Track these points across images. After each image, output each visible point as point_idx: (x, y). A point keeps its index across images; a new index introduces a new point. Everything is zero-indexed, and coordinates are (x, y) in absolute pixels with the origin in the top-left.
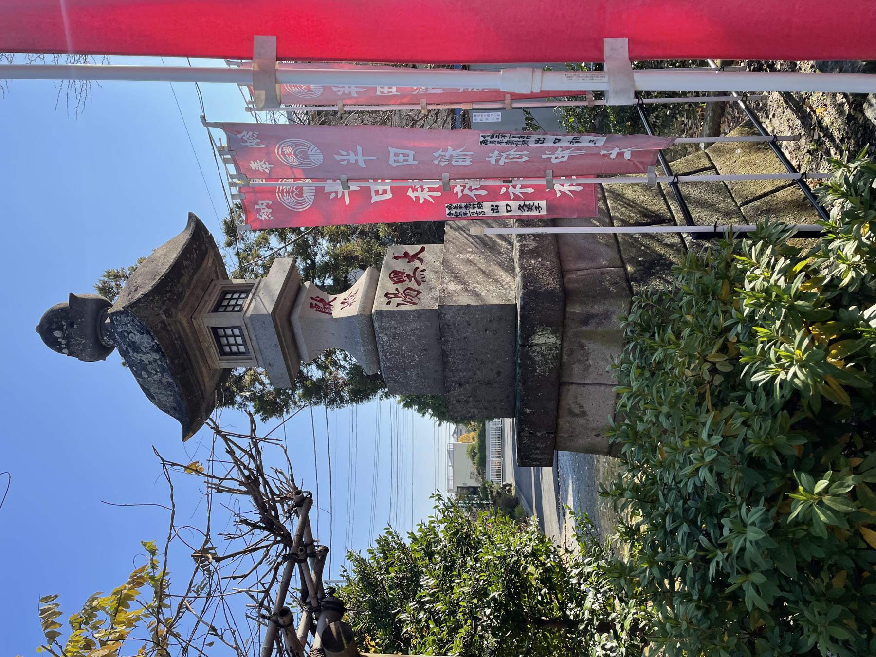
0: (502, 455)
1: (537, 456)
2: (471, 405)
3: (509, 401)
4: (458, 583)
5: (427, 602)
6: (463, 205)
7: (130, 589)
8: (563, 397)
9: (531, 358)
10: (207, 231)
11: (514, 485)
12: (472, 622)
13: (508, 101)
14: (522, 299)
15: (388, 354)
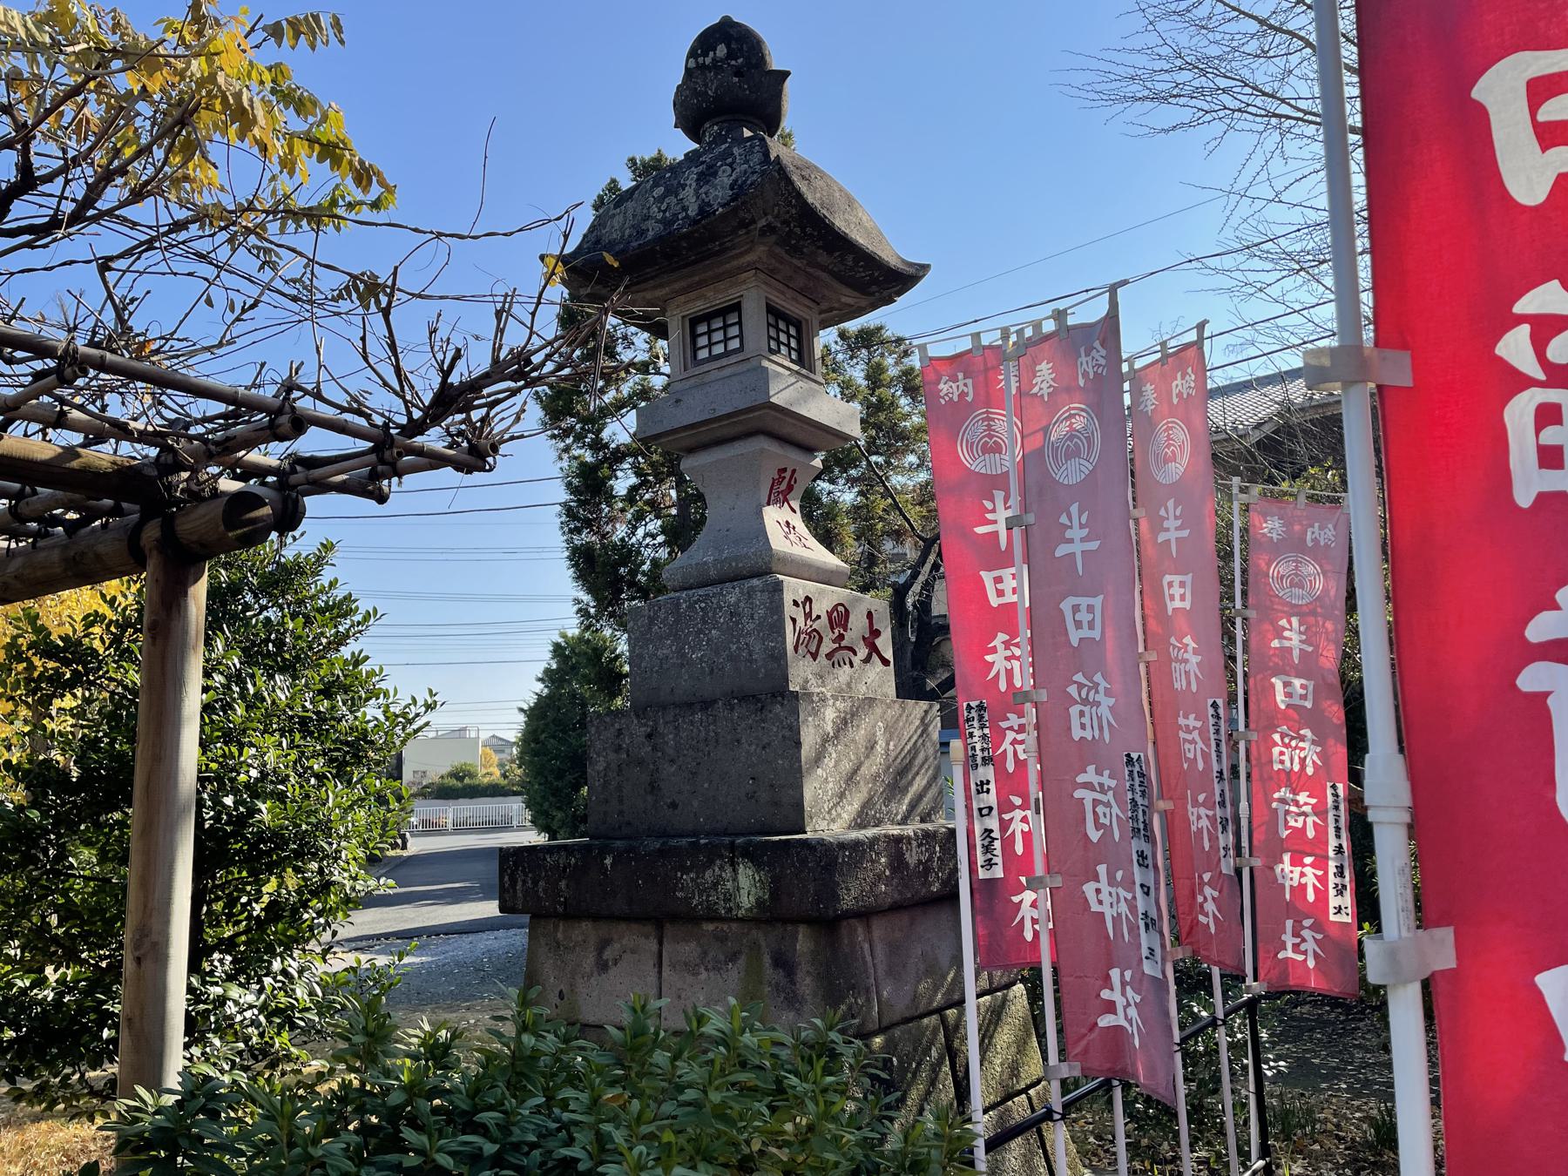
0: (460, 828)
1: (520, 883)
2: (612, 756)
3: (620, 827)
4: (280, 744)
5: (244, 689)
6: (987, 731)
7: (350, 163)
8: (634, 926)
9: (711, 863)
10: (900, 294)
11: (405, 854)
12: (212, 771)
13: (1162, 805)
14: (821, 842)
15: (703, 605)
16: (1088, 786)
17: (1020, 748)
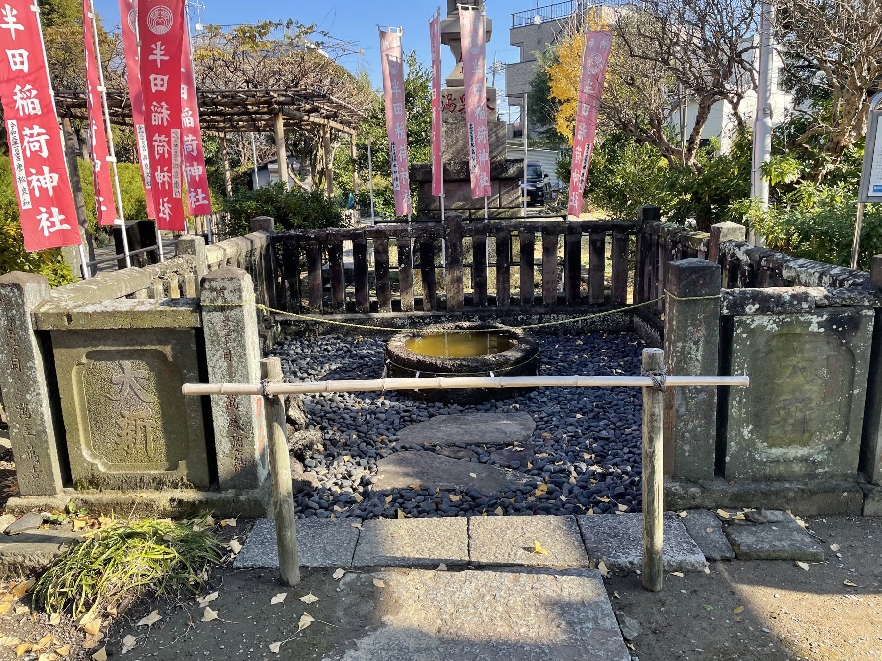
16: (156, 141)
17: (32, 145)
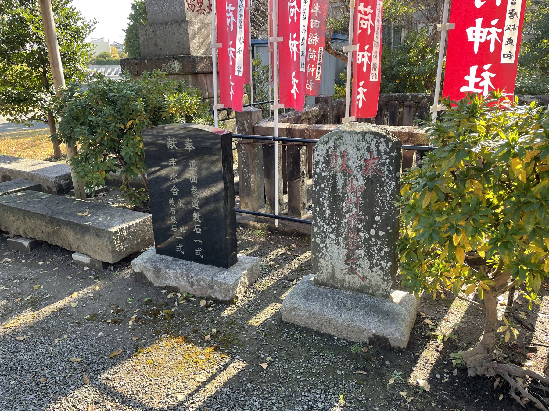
2: (145, 37)
